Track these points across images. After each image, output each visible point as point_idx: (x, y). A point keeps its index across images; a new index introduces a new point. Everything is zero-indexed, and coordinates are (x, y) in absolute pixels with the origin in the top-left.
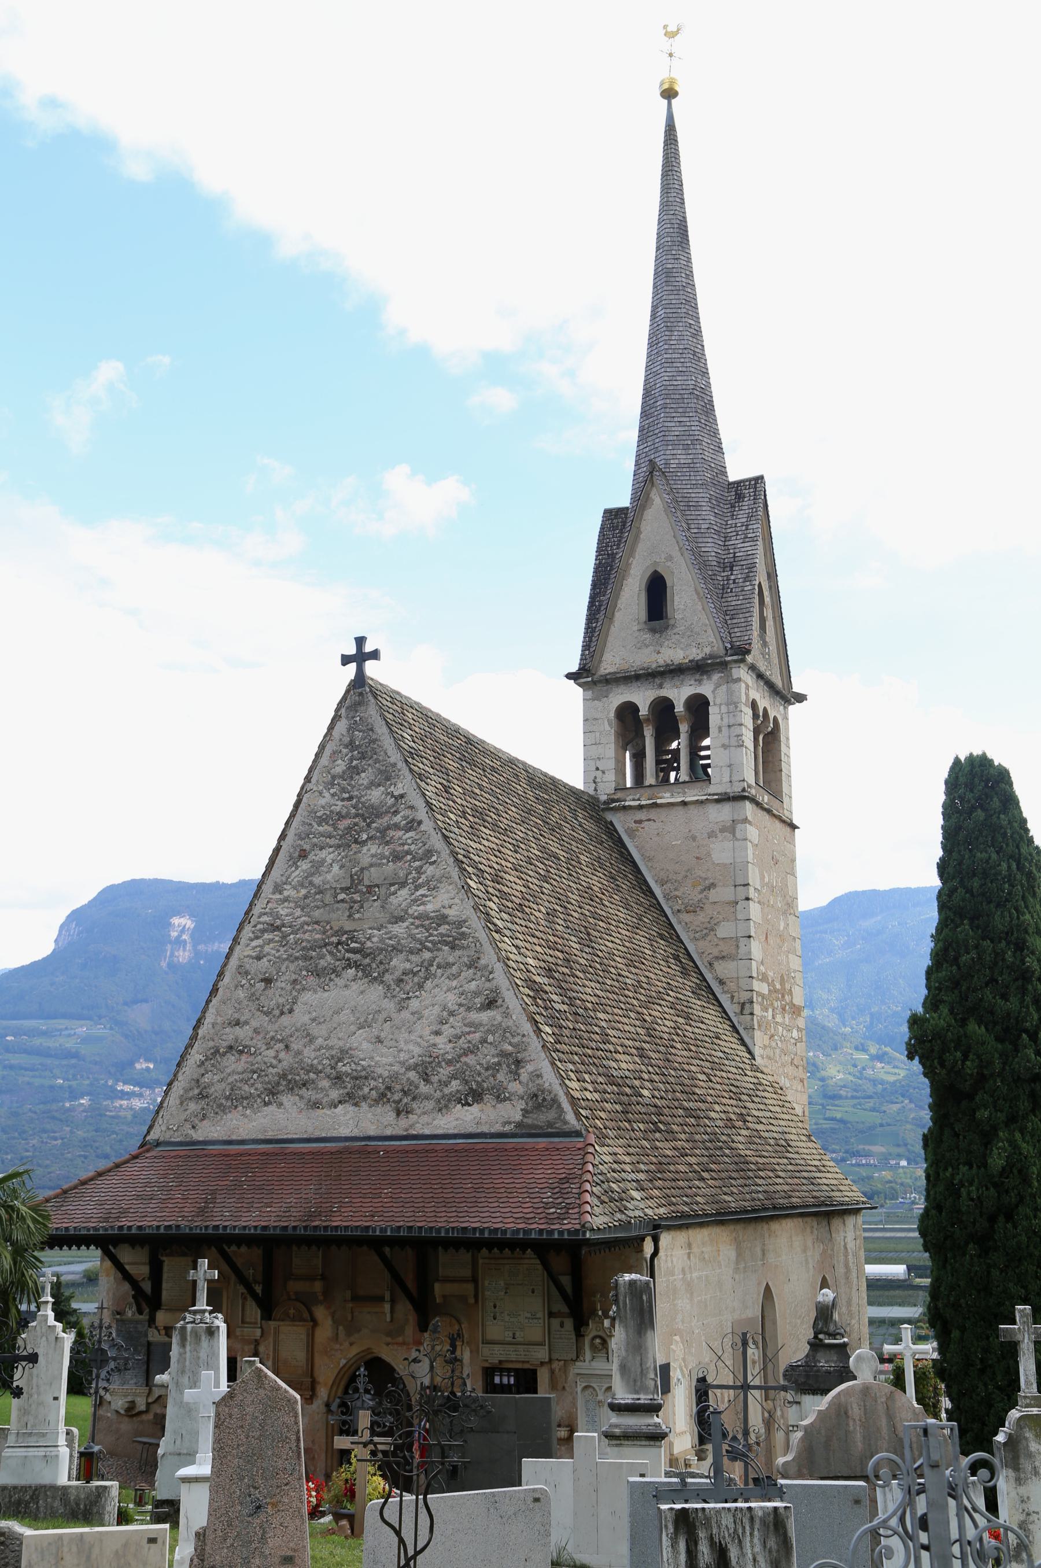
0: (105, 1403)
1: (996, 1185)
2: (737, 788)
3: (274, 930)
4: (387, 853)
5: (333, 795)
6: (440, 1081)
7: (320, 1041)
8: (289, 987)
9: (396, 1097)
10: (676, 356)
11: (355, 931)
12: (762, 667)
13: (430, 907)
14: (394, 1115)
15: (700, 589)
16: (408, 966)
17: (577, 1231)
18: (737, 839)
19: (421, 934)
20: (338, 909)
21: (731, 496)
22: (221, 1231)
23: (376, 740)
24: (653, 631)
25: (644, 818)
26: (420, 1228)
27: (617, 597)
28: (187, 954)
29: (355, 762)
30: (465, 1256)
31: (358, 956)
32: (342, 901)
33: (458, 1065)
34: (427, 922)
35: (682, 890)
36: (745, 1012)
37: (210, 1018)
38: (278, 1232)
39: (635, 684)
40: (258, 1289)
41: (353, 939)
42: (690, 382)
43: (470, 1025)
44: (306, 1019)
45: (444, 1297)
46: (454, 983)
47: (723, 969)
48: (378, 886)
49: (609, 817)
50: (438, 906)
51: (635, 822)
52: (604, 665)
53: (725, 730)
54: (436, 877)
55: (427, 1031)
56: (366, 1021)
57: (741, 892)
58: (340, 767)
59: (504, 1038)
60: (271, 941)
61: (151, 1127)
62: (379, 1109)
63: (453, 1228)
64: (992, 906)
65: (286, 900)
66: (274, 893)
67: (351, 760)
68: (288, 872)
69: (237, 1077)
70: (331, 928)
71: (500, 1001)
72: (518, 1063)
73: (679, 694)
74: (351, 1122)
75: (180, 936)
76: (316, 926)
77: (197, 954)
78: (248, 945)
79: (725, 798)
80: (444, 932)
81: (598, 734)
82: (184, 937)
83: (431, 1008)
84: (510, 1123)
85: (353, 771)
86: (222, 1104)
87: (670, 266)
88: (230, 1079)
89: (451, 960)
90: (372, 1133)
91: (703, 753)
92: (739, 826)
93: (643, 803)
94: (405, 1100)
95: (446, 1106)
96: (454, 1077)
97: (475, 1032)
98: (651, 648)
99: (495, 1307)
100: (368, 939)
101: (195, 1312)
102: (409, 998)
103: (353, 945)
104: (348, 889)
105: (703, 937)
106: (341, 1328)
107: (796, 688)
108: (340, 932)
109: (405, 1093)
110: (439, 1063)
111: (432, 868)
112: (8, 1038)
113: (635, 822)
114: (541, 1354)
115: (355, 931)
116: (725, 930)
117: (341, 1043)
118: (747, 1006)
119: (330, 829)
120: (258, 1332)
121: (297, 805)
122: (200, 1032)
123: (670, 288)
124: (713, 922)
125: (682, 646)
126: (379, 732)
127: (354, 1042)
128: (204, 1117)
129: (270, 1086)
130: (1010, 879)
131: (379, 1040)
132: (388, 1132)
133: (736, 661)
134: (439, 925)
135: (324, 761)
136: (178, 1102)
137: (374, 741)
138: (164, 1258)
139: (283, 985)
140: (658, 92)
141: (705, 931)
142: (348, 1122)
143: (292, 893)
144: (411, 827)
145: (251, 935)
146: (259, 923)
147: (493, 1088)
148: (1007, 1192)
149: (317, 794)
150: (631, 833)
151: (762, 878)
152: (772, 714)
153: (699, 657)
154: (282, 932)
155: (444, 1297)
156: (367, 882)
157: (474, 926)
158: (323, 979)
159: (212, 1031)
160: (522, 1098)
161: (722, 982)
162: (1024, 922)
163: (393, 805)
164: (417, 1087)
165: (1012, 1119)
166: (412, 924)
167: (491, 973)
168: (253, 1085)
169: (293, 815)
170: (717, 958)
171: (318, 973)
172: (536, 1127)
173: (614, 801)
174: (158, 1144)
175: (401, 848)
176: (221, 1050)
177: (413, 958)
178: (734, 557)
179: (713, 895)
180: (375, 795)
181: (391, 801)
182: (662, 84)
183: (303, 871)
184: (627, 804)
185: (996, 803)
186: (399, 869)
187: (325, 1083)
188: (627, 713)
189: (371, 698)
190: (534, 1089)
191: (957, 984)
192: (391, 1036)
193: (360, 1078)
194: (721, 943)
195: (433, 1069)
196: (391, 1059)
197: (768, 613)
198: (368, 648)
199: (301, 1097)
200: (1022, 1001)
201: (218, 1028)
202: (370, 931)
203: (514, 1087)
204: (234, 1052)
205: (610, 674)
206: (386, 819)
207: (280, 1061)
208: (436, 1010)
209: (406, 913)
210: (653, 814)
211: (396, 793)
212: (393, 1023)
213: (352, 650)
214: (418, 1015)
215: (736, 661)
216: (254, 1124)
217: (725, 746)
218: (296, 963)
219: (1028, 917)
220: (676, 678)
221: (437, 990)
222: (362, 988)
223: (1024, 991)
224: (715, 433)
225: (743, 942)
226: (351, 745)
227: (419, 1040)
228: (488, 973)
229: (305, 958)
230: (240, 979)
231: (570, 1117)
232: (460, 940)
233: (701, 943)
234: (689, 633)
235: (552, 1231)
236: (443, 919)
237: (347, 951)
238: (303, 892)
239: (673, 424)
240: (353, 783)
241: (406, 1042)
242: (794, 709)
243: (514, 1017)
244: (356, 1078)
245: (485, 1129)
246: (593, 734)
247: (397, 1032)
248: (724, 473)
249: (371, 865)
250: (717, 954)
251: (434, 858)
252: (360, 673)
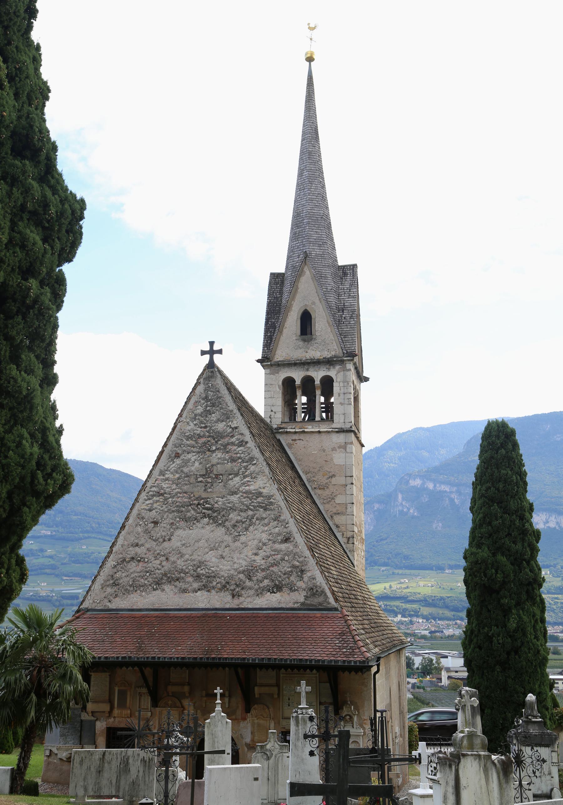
0: (53, 754)
1: (510, 637)
2: (348, 426)
3: (160, 496)
4: (227, 458)
5: (195, 425)
6: (257, 580)
7: (187, 556)
8: (168, 527)
9: (232, 588)
10: (314, 197)
11: (208, 498)
13: (252, 488)
14: (231, 597)
15: (330, 321)
16: (239, 518)
17: (364, 662)
18: (347, 452)
19: (247, 502)
20: (198, 486)
21: (340, 273)
22: (156, 660)
23: (221, 397)
24: (304, 341)
25: (297, 438)
26: (275, 659)
27: (285, 321)
29: (208, 408)
30: (273, 672)
31: (210, 512)
32: (201, 482)
33: (268, 572)
34: (251, 495)
35: (317, 477)
36: (350, 542)
37: (120, 542)
38: (191, 660)
39: (293, 368)
41: (207, 502)
42: (321, 212)
43: (275, 550)
44: (179, 544)
45: (260, 694)
46: (266, 528)
47: (339, 519)
48: (222, 475)
49: (278, 436)
50: (257, 487)
51: (292, 440)
53: (342, 395)
54: (256, 472)
55: (250, 554)
56: (214, 547)
57: (349, 480)
58: (200, 410)
59: (294, 558)
60: (157, 501)
62: (222, 594)
63: (294, 659)
64: (509, 497)
65: (167, 479)
66: (159, 475)
67: (206, 406)
68: (168, 465)
69: (136, 574)
70: (194, 496)
71: (292, 539)
72: (302, 571)
73: (318, 375)
74: (205, 600)
76: (185, 494)
78: (144, 503)
79: (341, 431)
80: (260, 501)
81: (272, 393)
83: (252, 541)
84: (298, 603)
85: (207, 413)
86: (127, 589)
87: (311, 150)
88: (133, 576)
89: (264, 516)
90: (218, 606)
91: (324, 406)
92: (349, 446)
93: (297, 430)
94: (238, 589)
95: (261, 593)
96: (266, 578)
97: (277, 555)
98: (303, 350)
99: (289, 699)
100: (216, 503)
101: (302, 709)
102: (240, 535)
103: (207, 506)
104: (204, 475)
105: (328, 503)
106: (199, 711)
107: (365, 374)
110: (257, 570)
111: (253, 467)
113: (292, 440)
115: (208, 498)
116: (340, 499)
117: (200, 558)
118: (351, 539)
119: (193, 443)
120: (149, 714)
121: (174, 429)
122: (114, 549)
123: (311, 161)
124: (334, 495)
125: (319, 350)
126: (223, 393)
127: (207, 557)
129: (157, 580)
130: (517, 484)
131: (222, 557)
132: (227, 606)
133: (348, 360)
134: (257, 497)
135: (190, 406)
136: (100, 587)
137: (220, 397)
138: (92, 674)
139: (165, 525)
140: (304, 59)
141: (329, 499)
142: (203, 600)
143: (171, 476)
144: (241, 445)
145: (146, 497)
146: (151, 491)
147: (288, 584)
148: (516, 640)
149: (186, 423)
150: (290, 446)
153: (329, 356)
154: (164, 497)
155: (260, 694)
156: (215, 472)
157: (277, 498)
158: (189, 523)
159: (121, 549)
160: (305, 590)
161: (337, 526)
162: (524, 506)
163: (231, 432)
164: (244, 583)
165: (518, 604)
166: (242, 496)
167: (287, 524)
168: (146, 579)
169: (171, 434)
170: (335, 514)
171: (186, 520)
172: (313, 605)
173: (281, 428)
174: (88, 610)
175: (235, 455)
176: (127, 560)
177: (242, 514)
178: (344, 305)
179: (334, 480)
180: (221, 426)
181: (229, 430)
182: (306, 54)
183: (177, 464)
184: (288, 430)
185: (510, 446)
186: (235, 466)
187: (190, 579)
188: (289, 384)
189: (218, 374)
190: (311, 586)
191: (490, 535)
192: (229, 555)
193: (211, 577)
194: (337, 506)
195: (254, 574)
196: (229, 567)
198: (216, 348)
199: (176, 586)
200: (523, 545)
201: (125, 547)
202: (217, 499)
203: (300, 584)
204: (135, 561)
205: (280, 361)
206: (227, 439)
207: (163, 567)
208: (256, 542)
209: (238, 490)
210: (302, 436)
211: (233, 426)
212: (230, 548)
213: (207, 348)
214: (245, 544)
215: (348, 360)
216: (147, 600)
217: (341, 404)
218: (173, 514)
219: (525, 503)
220: (316, 366)
221: (256, 531)
222: (212, 529)
223: (523, 540)
224: (332, 239)
225: (349, 506)
226: (206, 398)
227: (245, 558)
228: (285, 524)
229: (178, 511)
230: (138, 521)
231: (332, 600)
232: (269, 505)
233: (327, 506)
234: (323, 343)
235: (351, 661)
236: (260, 494)
237: (204, 509)
238: (177, 476)
239: (313, 233)
240: (207, 419)
241: (238, 559)
242: (363, 385)
243: (300, 548)
244: (209, 577)
245: (283, 606)
246: (270, 392)
247: (233, 553)
248: (336, 261)
249: (218, 464)
250: (335, 512)
251: (255, 462)
252: (211, 361)
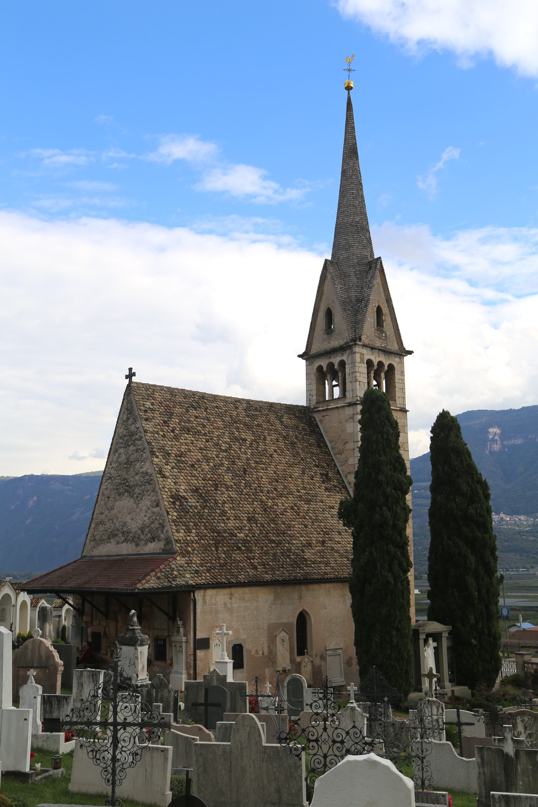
9: (136, 540)
28: (498, 446)
37: (95, 512)
40: (103, 609)
52: (312, 350)
53: (351, 374)
61: (83, 551)
73: (336, 360)
75: (494, 438)
77: (504, 446)
82: (496, 438)
85: (128, 419)
96: (149, 532)
108: (125, 479)
112: (415, 491)
114: (166, 633)
120: (105, 624)
128: (95, 547)
132: (134, 553)
135: (121, 416)
150: (321, 421)
152: (386, 363)
174: (84, 557)
180: (132, 428)
210: (328, 413)
226: (127, 409)
229: (117, 489)
236: (147, 473)
250: (348, 471)
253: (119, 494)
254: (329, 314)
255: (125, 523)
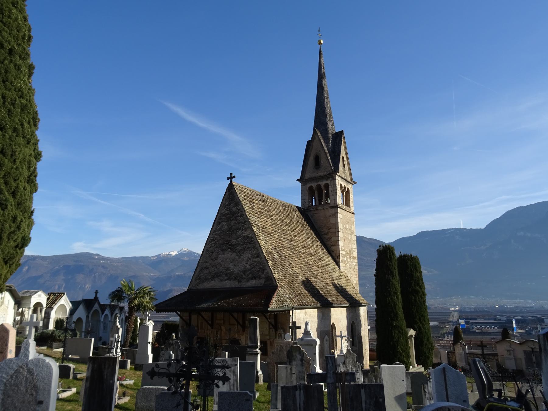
12: (343, 176)
19: (243, 241)
40: (210, 322)
85: (230, 204)
96: (250, 274)
108: (227, 241)
109: (240, 277)
131: (235, 265)
142: (228, 284)
151: (343, 226)
187: (224, 276)
188: (311, 188)
197: (346, 163)
203: (263, 276)
214: (243, 259)
236: (248, 237)
252: (231, 182)
253: (223, 250)
254: (317, 159)
255: (227, 268)
